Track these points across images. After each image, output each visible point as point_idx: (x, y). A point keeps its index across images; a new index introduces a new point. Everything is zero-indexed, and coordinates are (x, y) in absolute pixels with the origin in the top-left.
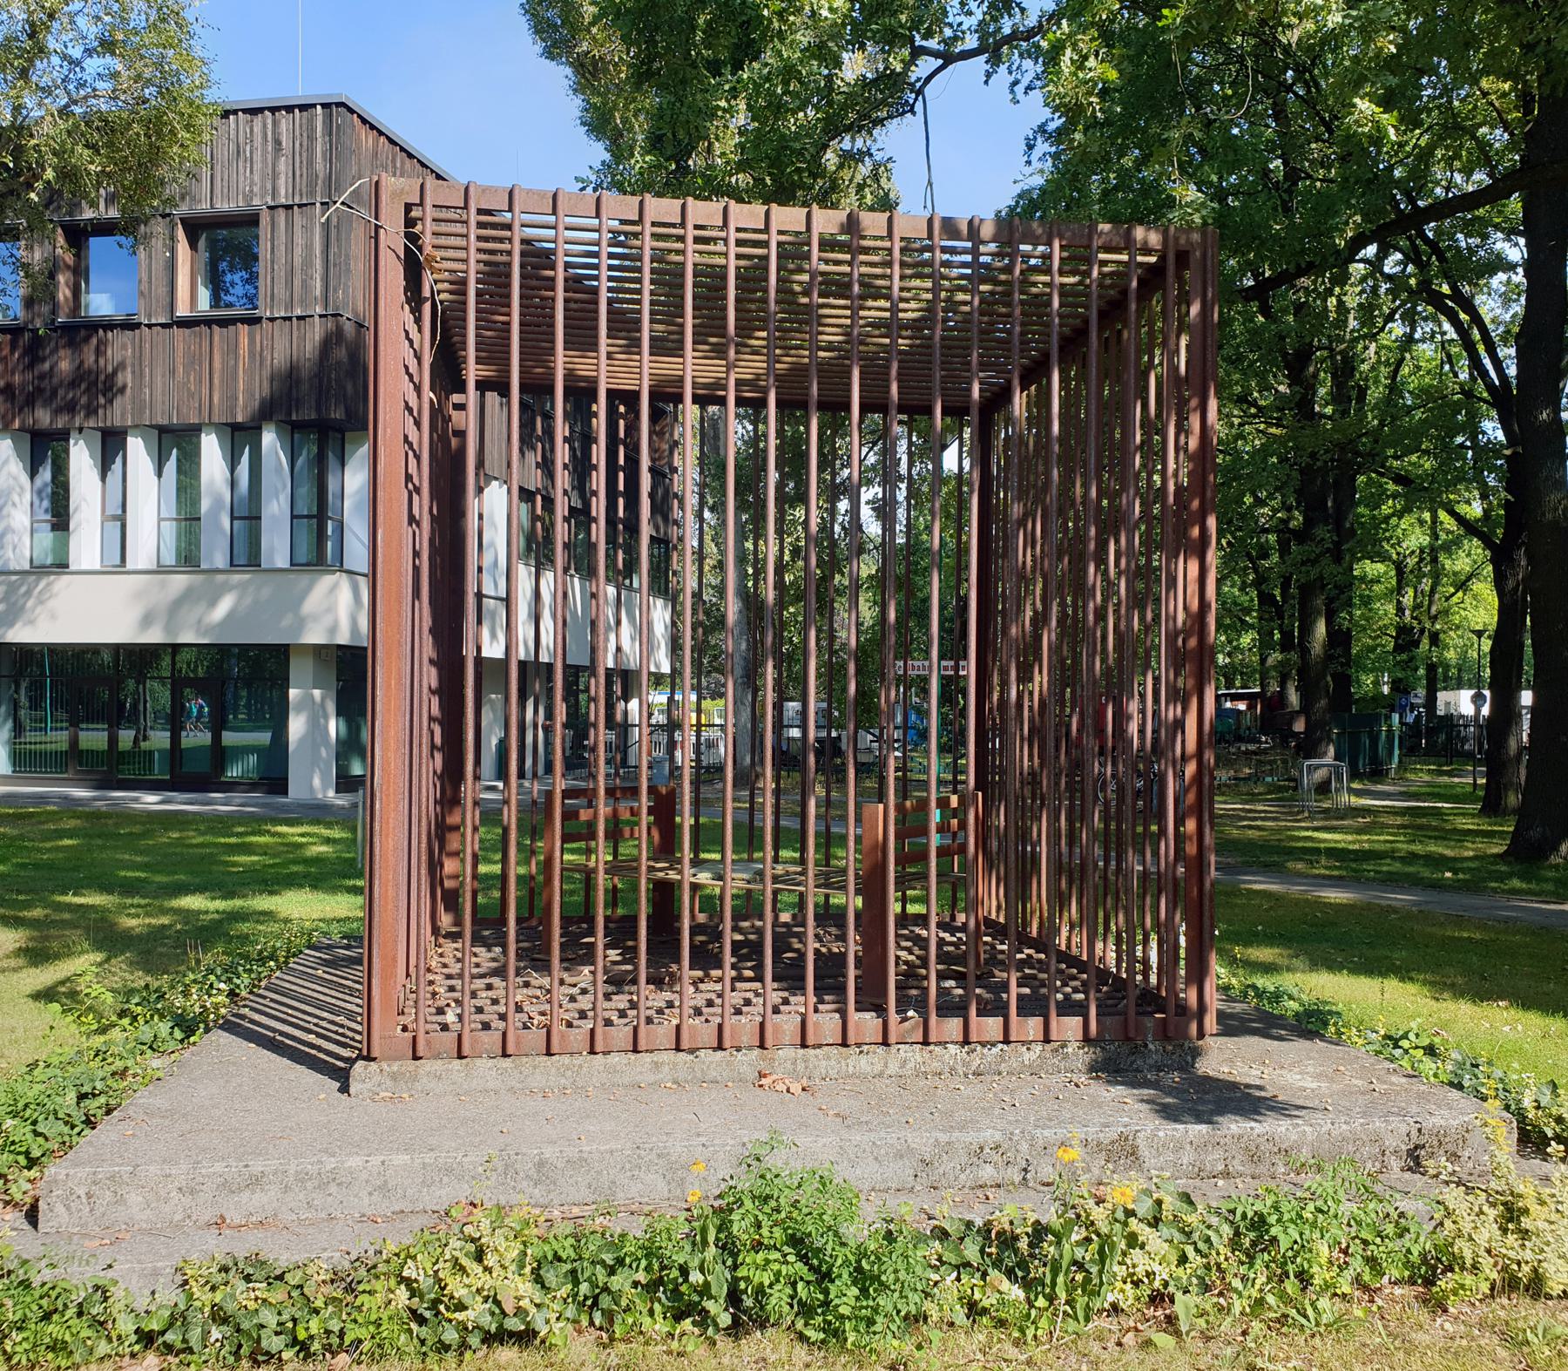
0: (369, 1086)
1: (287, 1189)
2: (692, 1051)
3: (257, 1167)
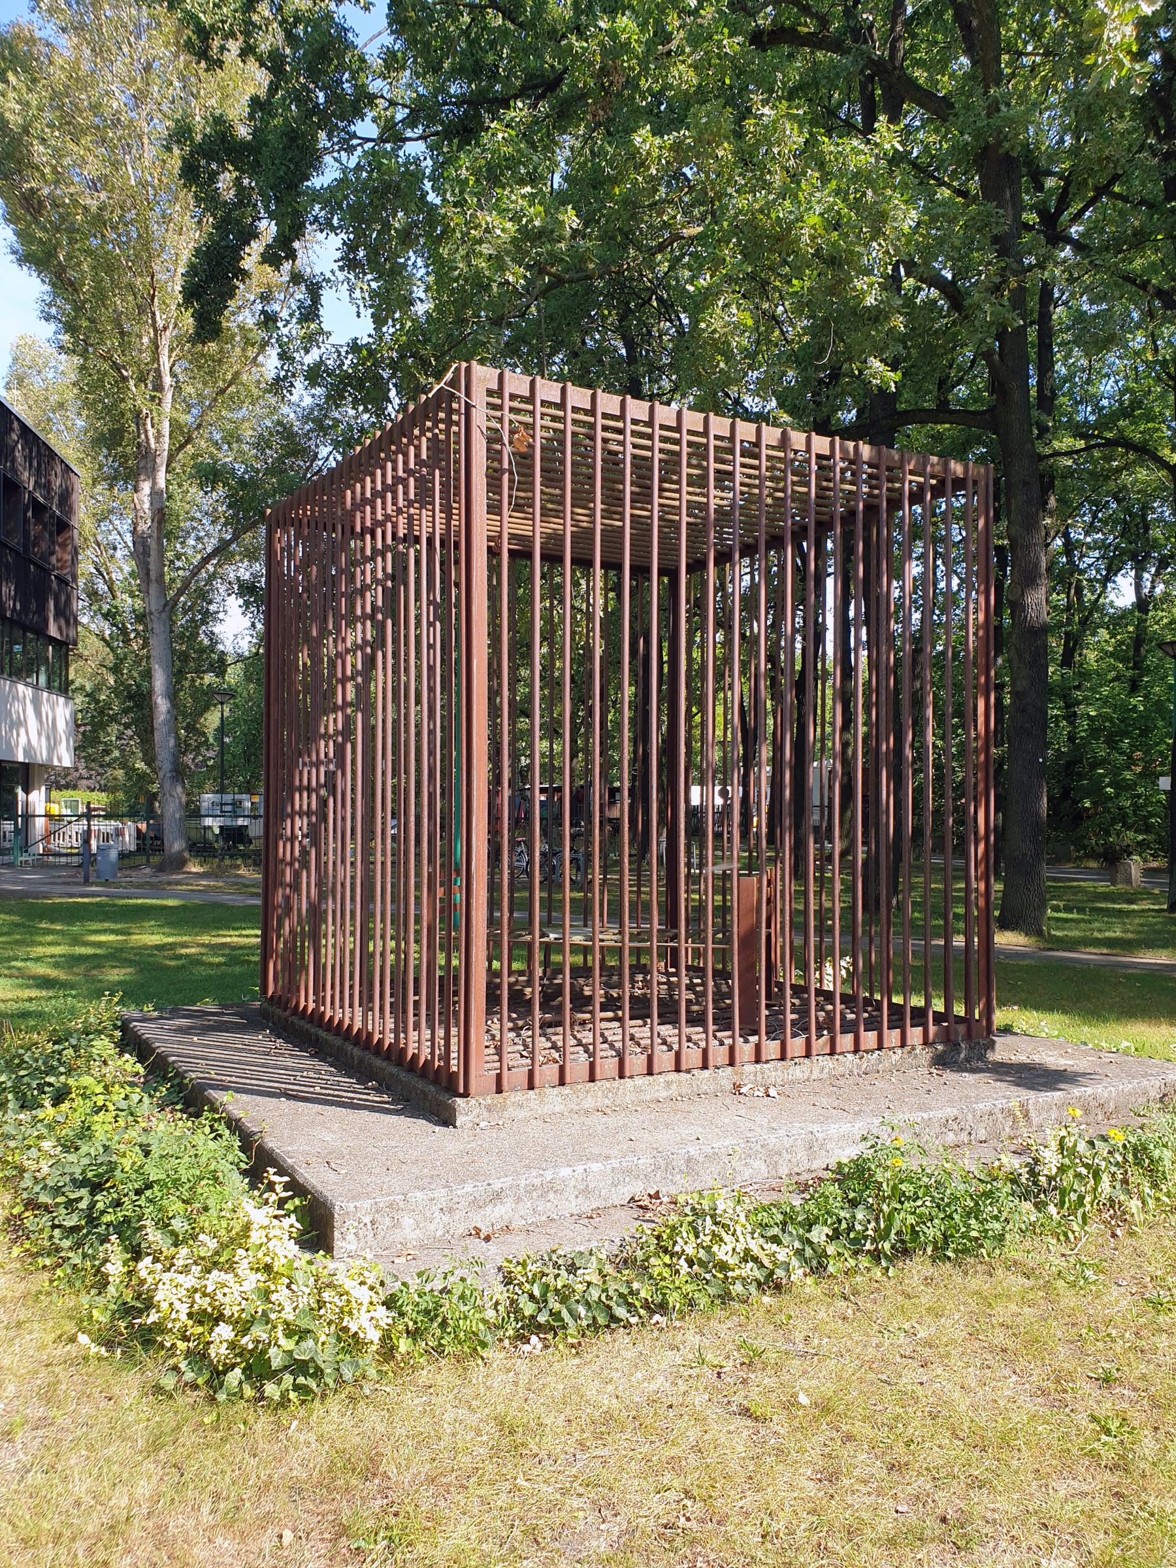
0: (470, 1118)
1: (519, 1200)
2: (688, 1071)
3: (497, 1186)
